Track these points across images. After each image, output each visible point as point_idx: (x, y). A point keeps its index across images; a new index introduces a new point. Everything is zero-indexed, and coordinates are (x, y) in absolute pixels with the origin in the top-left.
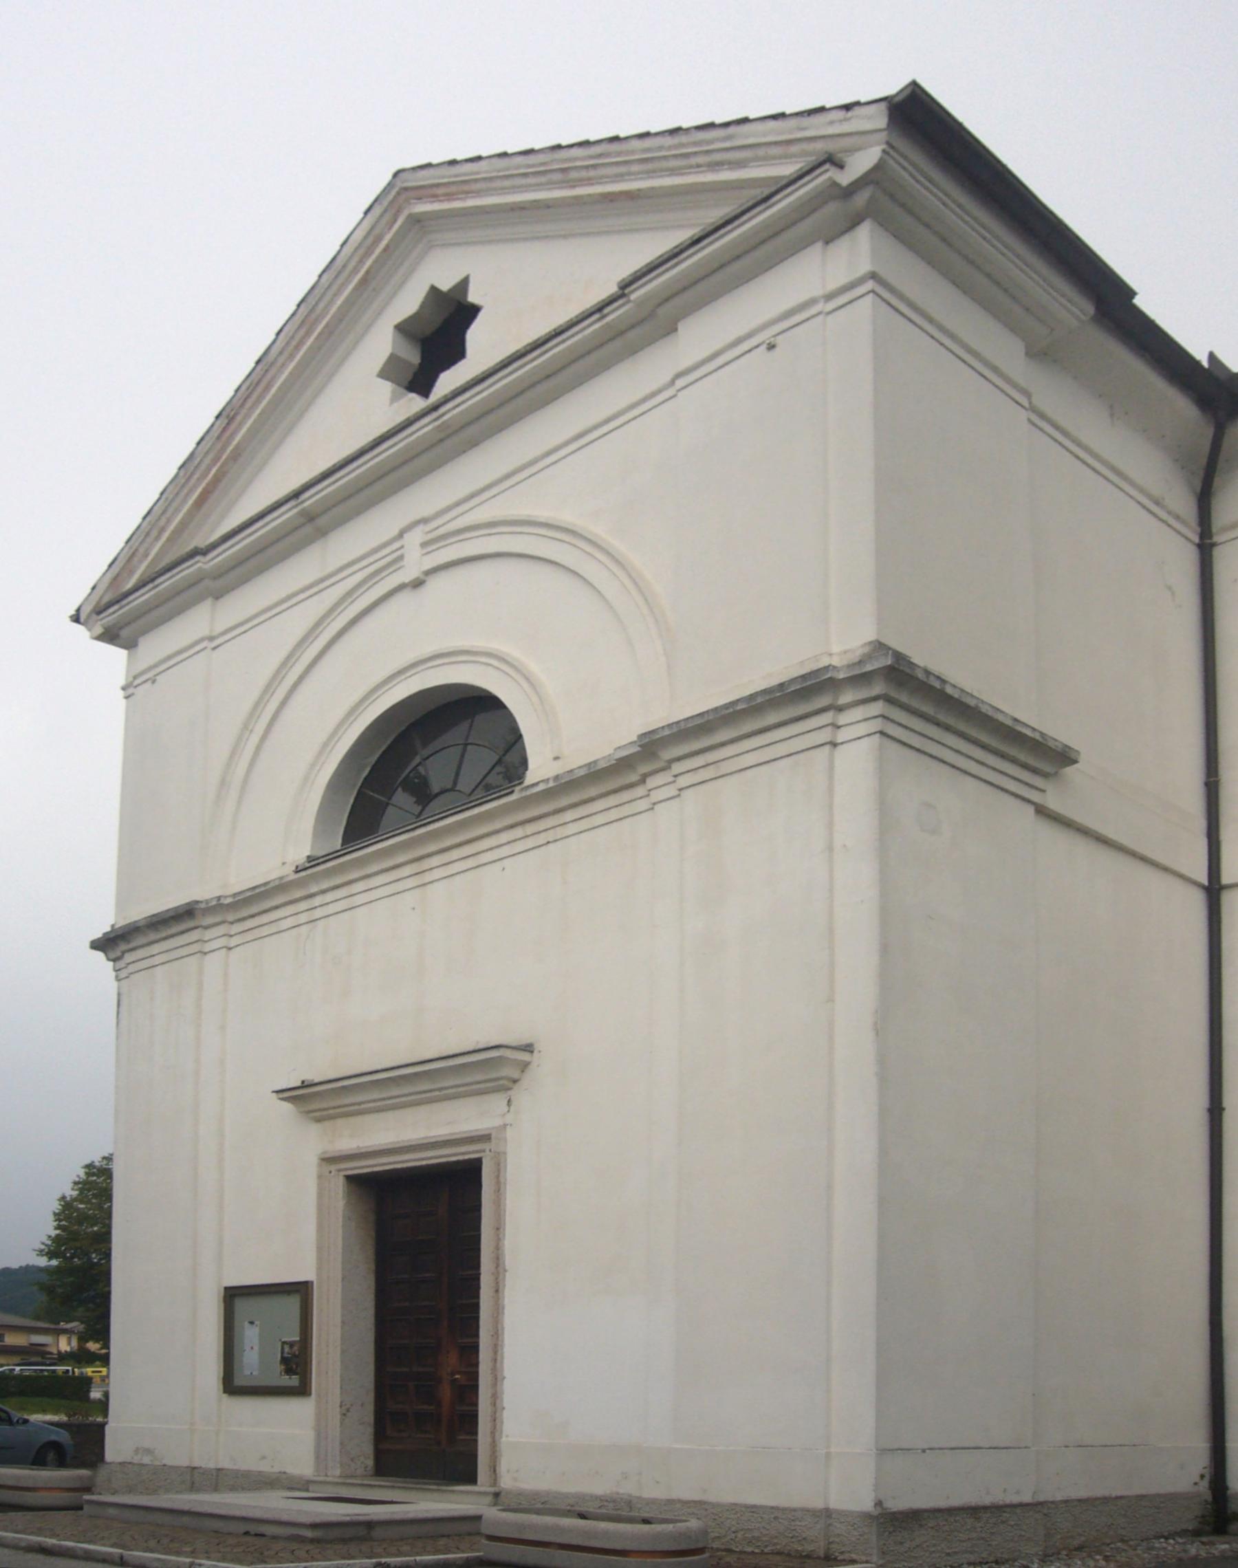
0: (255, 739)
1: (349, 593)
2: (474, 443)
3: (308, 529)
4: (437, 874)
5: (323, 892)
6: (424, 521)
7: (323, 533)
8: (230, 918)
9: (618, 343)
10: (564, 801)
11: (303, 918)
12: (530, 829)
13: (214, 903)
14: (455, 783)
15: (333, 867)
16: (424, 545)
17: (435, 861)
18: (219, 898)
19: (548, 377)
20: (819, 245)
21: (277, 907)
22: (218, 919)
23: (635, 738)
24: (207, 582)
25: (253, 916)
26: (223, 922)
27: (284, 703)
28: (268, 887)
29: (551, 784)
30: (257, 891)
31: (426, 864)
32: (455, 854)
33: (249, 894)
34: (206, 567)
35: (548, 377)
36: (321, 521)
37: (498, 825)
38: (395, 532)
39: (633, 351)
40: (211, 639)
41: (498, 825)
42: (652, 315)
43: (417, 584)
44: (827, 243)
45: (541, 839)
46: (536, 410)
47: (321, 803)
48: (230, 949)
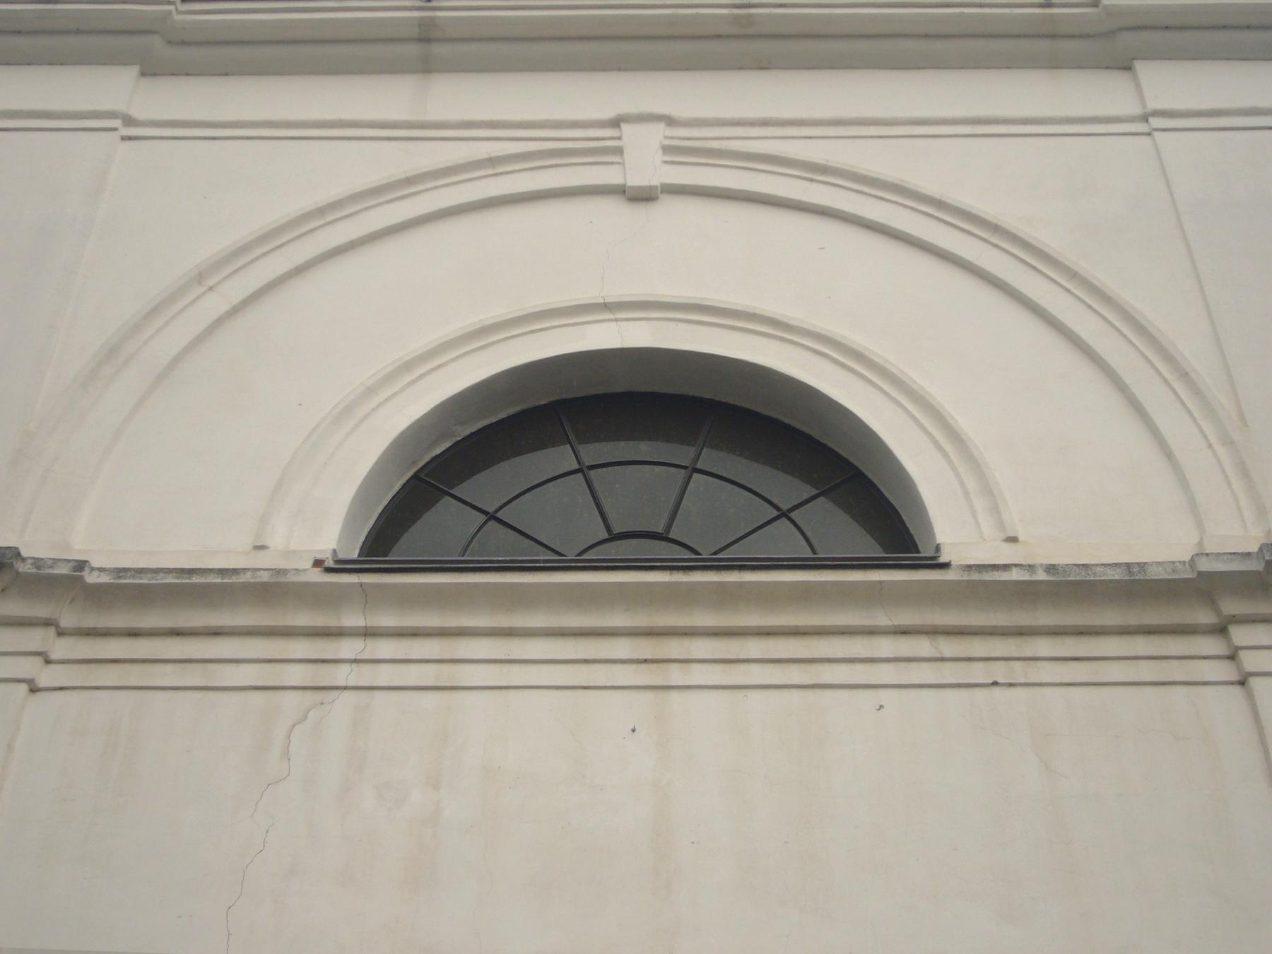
0: (215, 305)
1: (492, 161)
2: (763, 65)
3: (413, 50)
4: (700, 674)
5: (368, 633)
6: (670, 121)
7: (426, 67)
8: (68, 620)
9: (1045, 44)
10: (1044, 617)
11: (295, 674)
12: (948, 647)
13: (63, 570)
14: (669, 526)
15: (440, 587)
16: (667, 149)
17: (702, 648)
18: (81, 565)
19: (926, 36)
20: (134, 70)
21: (216, 633)
22: (41, 611)
23: (1254, 548)
24: (156, 41)
25: (134, 634)
26: (47, 623)
27: (299, 271)
28: (234, 579)
29: (1041, 576)
30: (196, 579)
31: (675, 648)
32: (754, 648)
33: (170, 580)
34: (177, 17)
35: (926, 36)
36: (439, 50)
37: (882, 619)
38: (609, 114)
39: (1054, 63)
40: (129, 121)
41: (882, 619)
42: (1110, 34)
43: (643, 196)
44: (143, 74)
45: (978, 673)
46: (310, 73)
47: (377, 463)
48: (34, 690)
